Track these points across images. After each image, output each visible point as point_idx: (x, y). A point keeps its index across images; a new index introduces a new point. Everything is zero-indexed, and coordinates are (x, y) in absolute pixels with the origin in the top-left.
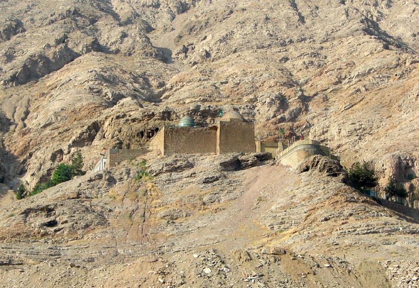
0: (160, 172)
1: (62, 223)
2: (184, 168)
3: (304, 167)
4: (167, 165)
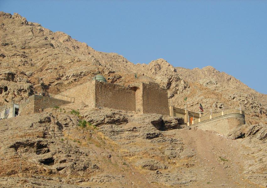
0: (102, 123)
1: (61, 162)
2: (122, 121)
3: (238, 133)
4: (107, 117)
